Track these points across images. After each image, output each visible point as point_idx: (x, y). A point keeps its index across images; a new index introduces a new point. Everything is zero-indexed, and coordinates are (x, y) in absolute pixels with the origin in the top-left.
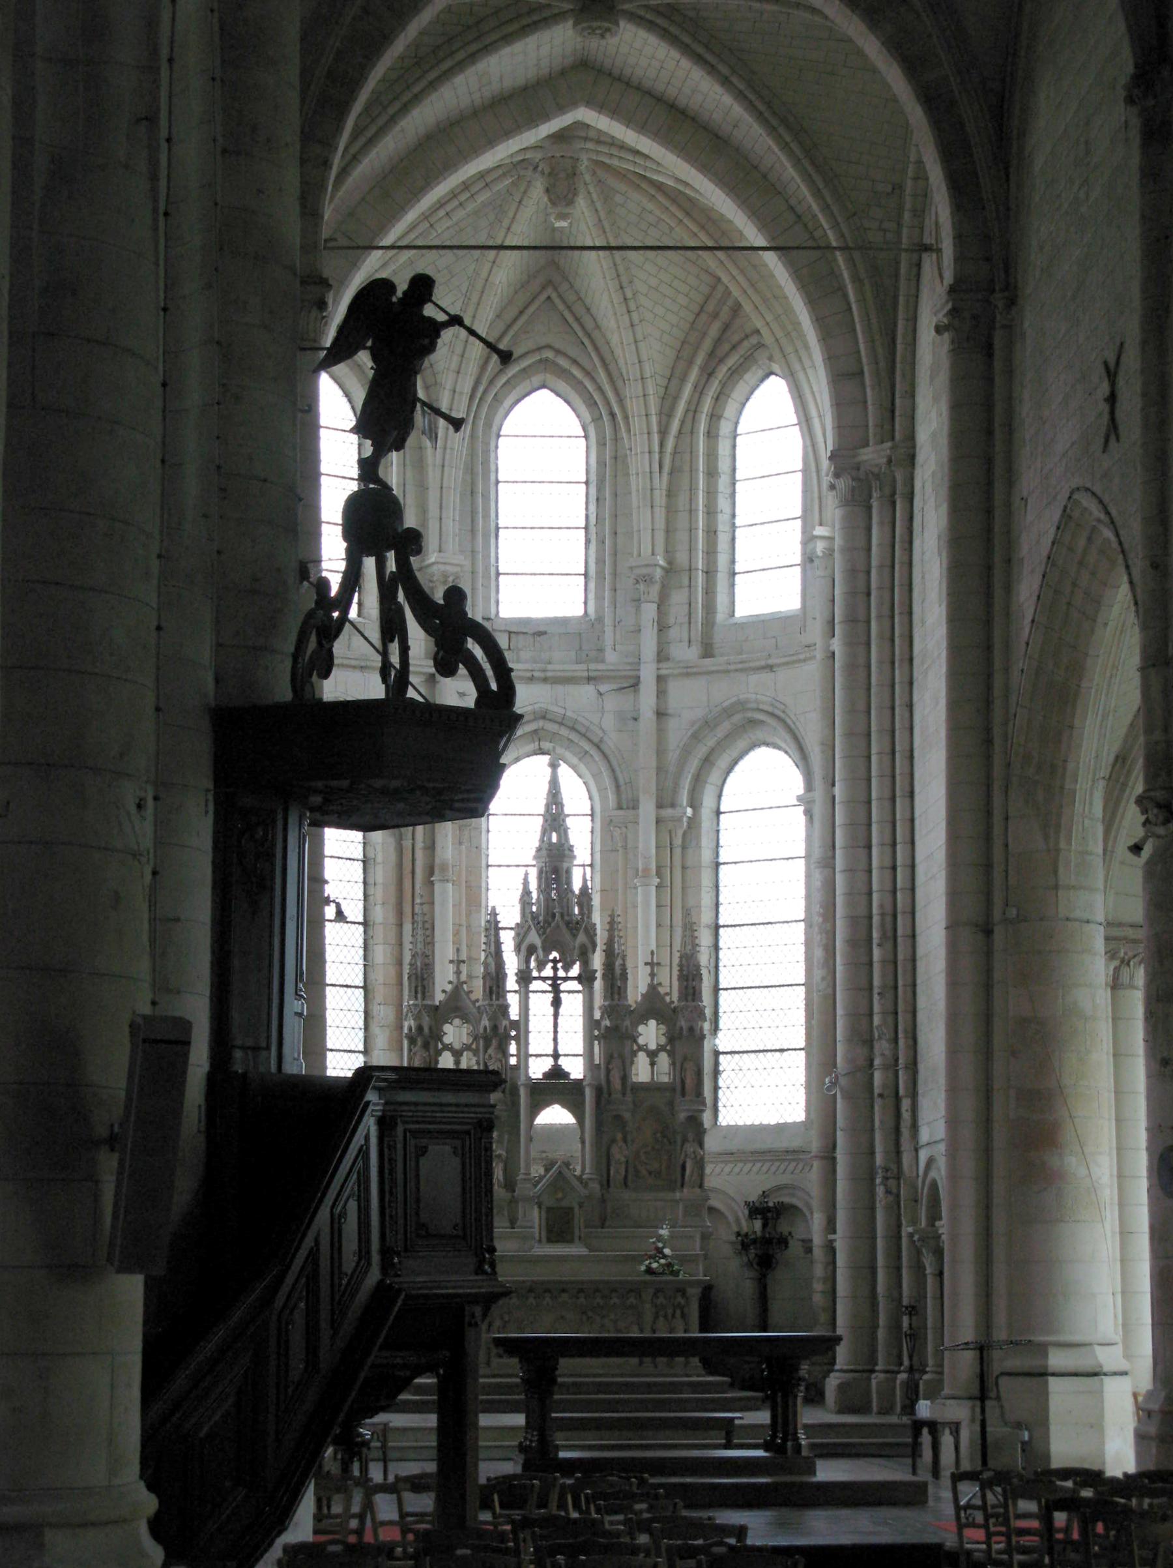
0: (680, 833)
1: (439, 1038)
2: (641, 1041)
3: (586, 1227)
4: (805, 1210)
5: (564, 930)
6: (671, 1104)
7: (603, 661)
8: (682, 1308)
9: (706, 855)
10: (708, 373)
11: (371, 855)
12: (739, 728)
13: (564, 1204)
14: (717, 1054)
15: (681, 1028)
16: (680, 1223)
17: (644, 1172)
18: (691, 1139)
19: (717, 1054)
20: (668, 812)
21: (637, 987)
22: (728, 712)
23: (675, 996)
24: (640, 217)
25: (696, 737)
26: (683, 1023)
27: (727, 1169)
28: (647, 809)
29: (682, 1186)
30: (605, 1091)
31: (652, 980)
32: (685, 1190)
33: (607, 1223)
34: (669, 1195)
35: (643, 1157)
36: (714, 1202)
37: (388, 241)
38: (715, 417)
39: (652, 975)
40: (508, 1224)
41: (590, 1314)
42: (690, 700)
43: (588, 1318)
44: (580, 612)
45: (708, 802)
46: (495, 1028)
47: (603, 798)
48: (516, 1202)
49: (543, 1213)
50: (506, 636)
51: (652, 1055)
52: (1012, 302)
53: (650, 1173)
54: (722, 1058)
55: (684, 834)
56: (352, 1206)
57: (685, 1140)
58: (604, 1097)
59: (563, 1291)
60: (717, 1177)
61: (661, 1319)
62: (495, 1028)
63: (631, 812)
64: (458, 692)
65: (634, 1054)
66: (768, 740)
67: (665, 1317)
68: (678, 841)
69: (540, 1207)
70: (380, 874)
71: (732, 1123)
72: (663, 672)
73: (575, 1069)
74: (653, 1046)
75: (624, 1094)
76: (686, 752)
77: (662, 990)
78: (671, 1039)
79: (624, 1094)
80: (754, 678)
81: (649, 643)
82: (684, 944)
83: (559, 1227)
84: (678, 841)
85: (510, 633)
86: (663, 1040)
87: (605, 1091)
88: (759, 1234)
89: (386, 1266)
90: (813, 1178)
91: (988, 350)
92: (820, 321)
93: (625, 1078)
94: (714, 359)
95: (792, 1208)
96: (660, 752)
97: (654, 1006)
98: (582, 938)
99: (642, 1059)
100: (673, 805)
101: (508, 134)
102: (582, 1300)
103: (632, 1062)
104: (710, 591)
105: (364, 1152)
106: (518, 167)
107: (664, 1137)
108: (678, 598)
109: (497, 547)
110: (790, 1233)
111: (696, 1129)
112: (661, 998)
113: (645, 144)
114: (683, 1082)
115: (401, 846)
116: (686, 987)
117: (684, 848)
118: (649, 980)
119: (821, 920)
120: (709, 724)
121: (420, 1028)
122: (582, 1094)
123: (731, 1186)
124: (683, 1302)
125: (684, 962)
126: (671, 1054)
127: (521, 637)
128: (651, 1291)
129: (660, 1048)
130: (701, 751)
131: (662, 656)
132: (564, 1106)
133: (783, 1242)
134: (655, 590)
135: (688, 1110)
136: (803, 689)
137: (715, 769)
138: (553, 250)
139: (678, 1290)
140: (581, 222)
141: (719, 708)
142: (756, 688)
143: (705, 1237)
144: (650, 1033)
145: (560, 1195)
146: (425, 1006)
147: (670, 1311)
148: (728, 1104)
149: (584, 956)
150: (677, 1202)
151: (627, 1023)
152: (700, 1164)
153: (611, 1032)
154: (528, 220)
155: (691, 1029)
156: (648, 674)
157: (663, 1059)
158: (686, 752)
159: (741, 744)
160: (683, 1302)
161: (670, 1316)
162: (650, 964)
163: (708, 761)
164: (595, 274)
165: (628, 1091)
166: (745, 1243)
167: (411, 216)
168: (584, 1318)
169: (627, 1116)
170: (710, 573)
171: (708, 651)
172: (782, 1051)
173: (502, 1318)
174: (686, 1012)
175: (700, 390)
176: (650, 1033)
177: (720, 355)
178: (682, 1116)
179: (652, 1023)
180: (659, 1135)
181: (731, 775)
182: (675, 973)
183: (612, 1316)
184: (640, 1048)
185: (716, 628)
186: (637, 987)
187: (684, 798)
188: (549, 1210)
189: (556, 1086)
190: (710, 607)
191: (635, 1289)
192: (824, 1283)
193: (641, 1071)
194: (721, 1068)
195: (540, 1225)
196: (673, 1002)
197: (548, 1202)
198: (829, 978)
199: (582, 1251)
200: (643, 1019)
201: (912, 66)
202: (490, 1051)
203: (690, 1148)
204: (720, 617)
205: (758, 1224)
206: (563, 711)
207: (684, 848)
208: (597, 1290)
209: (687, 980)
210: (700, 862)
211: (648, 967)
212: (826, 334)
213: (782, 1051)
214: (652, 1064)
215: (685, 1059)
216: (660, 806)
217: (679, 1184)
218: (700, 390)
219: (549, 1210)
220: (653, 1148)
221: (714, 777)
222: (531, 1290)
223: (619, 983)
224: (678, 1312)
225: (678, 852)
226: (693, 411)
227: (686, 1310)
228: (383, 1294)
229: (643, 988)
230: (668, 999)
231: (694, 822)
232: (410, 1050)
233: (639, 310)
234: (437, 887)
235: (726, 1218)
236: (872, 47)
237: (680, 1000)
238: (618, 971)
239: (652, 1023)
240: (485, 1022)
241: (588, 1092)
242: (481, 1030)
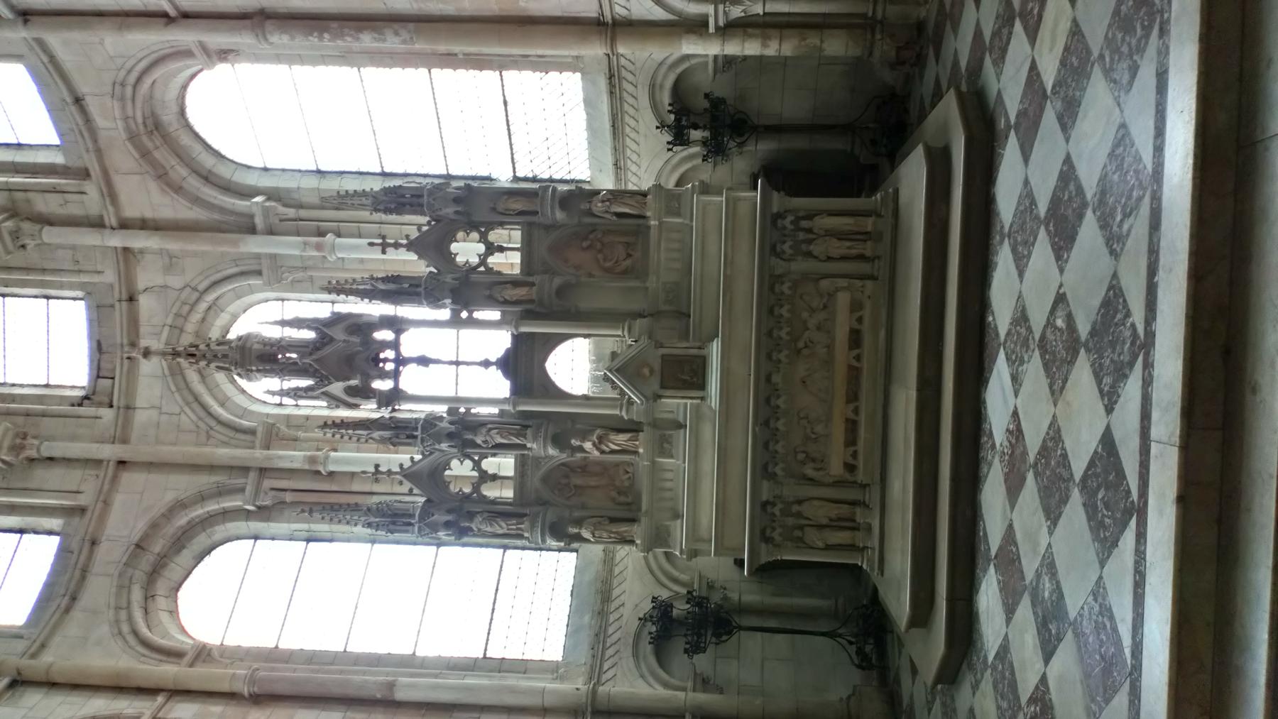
0: (281, 209)
1: (467, 497)
2: (475, 260)
3: (687, 339)
4: (679, 70)
5: (328, 350)
6: (549, 228)
7: (112, 286)
8: (799, 219)
9: (312, 182)
11: (305, 534)
12: (164, 140)
13: (657, 366)
14: (516, 179)
15: (456, 212)
16: (687, 222)
17: (628, 262)
18: (588, 206)
19: (516, 179)
20: (259, 221)
21: (411, 264)
22: (145, 154)
23: (423, 220)
26: (449, 211)
27: (634, 168)
28: (255, 245)
29: (644, 217)
30: (529, 307)
31: (401, 245)
32: (649, 214)
33: (685, 310)
34: (653, 234)
35: (608, 264)
36: (671, 185)
39: (397, 246)
40: (682, 431)
41: (801, 344)
43: (806, 347)
44: (81, 305)
45: (251, 180)
46: (450, 436)
47: (252, 291)
48: (655, 420)
49: (668, 393)
50: (101, 381)
51: (491, 249)
53: (629, 256)
54: (520, 174)
55: (285, 205)
57: (590, 213)
59: (768, 379)
60: (642, 178)
61: (812, 247)
62: (450, 436)
63: (263, 261)
65: (489, 271)
66: (175, 109)
67: (810, 242)
68: (291, 212)
69: (660, 397)
70: (322, 528)
71: (587, 164)
72: (114, 222)
73: (499, 342)
74: (481, 248)
75: (533, 284)
76: (197, 201)
77: (414, 233)
78: (471, 226)
79: (533, 284)
80: (100, 122)
81: (90, 238)
82: (362, 207)
83: (686, 374)
84: (291, 212)
85: (98, 377)
86: (475, 235)
87: (529, 307)
88: (707, 134)
90: (643, 55)
93: (515, 283)
95: (677, 89)
97: (434, 245)
98: (338, 334)
99: (495, 260)
100: (252, 216)
102: (782, 356)
103: (499, 273)
107: (586, 238)
109: (22, 386)
110: (707, 96)
112: (423, 235)
114: (521, 213)
115: (292, 503)
116: (412, 205)
117: (301, 206)
118: (403, 250)
119: (326, 35)
121: (447, 525)
122: (532, 335)
123: (651, 163)
124: (790, 218)
125: (381, 207)
126: (491, 226)
127: (103, 365)
128: (774, 261)
129: (483, 239)
130: (193, 183)
131: (97, 224)
132: (545, 360)
133: (716, 103)
134: (26, 226)
135: (552, 208)
137: (215, 170)
139: (774, 223)
141: (141, 161)
143: (705, 189)
144: (467, 250)
145: (646, 371)
146: (422, 518)
147: (801, 236)
148: (567, 169)
150: (661, 223)
151: (448, 279)
153: (463, 291)
155: (457, 200)
156: (116, 240)
157: (496, 236)
158: (197, 201)
159: (186, 140)
160: (790, 218)
161: (811, 236)
162: (384, 247)
163: (208, 178)
165: (531, 279)
166: (715, 150)
168: (805, 352)
169: (557, 281)
172: (505, 103)
173: (803, 463)
174: (458, 205)
176: (467, 250)
178: (560, 215)
179: (454, 247)
180: (585, 244)
181: (223, 153)
182: (393, 217)
183: (805, 315)
184: (483, 262)
185: (70, 165)
186: (411, 264)
187: (241, 204)
188: (663, 387)
189: (523, 365)
192: (769, 38)
193: (509, 262)
194: (530, 175)
195: (683, 398)
196: (429, 223)
197: (654, 385)
198: (396, 26)
199: (715, 349)
200: (450, 258)
202: (479, 441)
203: (598, 207)
204: (58, 159)
205: (696, 134)
206: (167, 329)
207: (301, 206)
208: (770, 334)
209: (404, 205)
210: (313, 189)
211: (388, 250)
213: (505, 103)
214: (501, 249)
215: (494, 209)
216: (252, 230)
217: (641, 221)
219: (663, 387)
220: (600, 251)
221: (224, 171)
222: (766, 423)
223: (406, 286)
224: (804, 224)
225: (303, 213)
227: (801, 214)
229: (413, 257)
230: (425, 228)
232: (475, 536)
234: (332, 468)
235: (687, 171)
237: (423, 214)
238: (391, 286)
239: (454, 247)
240: (444, 446)
241: (524, 329)
242: (455, 450)
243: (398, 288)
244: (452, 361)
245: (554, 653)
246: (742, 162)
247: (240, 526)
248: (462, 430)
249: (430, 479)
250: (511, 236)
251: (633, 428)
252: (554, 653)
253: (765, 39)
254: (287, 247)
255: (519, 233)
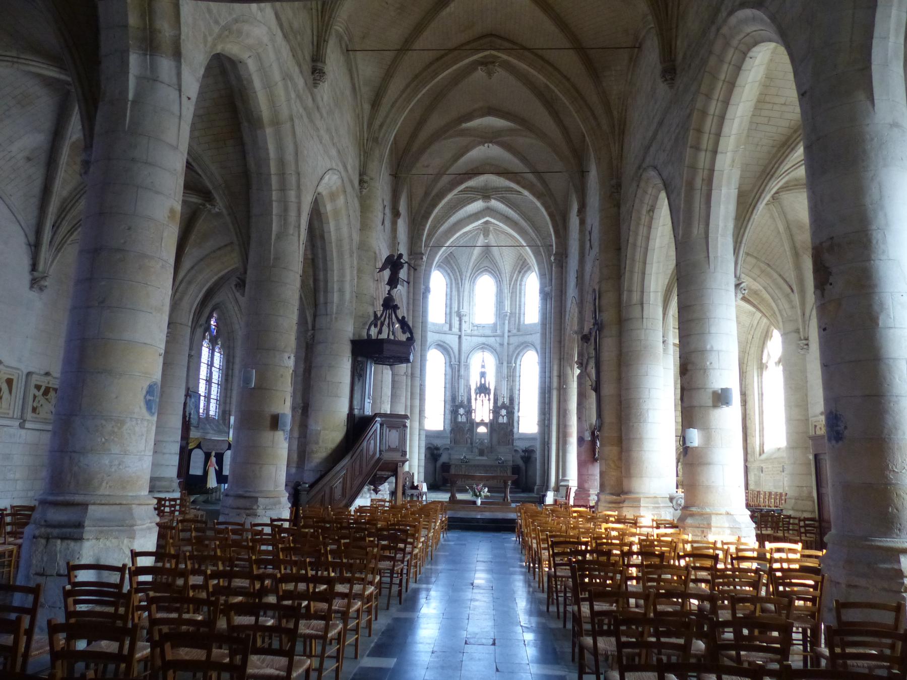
9: (518, 374)
10: (520, 272)
21: (499, 404)
22: (522, 344)
24: (503, 240)
25: (516, 349)
28: (505, 364)
37: (447, 244)
38: (521, 280)
42: (515, 341)
45: (518, 363)
52: (566, 257)
56: (372, 442)
58: (493, 426)
60: (516, 443)
64: (403, 337)
76: (514, 352)
83: (481, 453)
89: (380, 454)
91: (562, 267)
92: (537, 261)
94: (521, 269)
96: (508, 351)
97: (504, 406)
101: (472, 223)
104: (519, 318)
105: (376, 430)
106: (477, 229)
108: (513, 319)
111: (512, 432)
113: (501, 224)
120: (518, 346)
136: (537, 339)
138: (487, 246)
140: (492, 239)
142: (529, 338)
144: (461, 411)
149: (489, 394)
152: (513, 440)
153: (496, 411)
154: (481, 241)
158: (514, 352)
163: (518, 354)
164: (495, 251)
166: (522, 458)
167: (451, 240)
170: (520, 314)
171: (519, 330)
175: (518, 276)
176: (504, 412)
177: (522, 267)
186: (499, 404)
189: (482, 423)
190: (519, 321)
191: (497, 467)
193: (501, 420)
201: (547, 208)
212: (538, 264)
218: (518, 276)
226: (516, 280)
228: (379, 459)
231: (515, 367)
233: (506, 259)
236: (539, 204)
243: (496, 401)
244: (482, 411)
245: (520, 431)
246: (520, 463)
247: (448, 361)
248: (469, 412)
249: (461, 405)
250: (505, 420)
251: (471, 444)
252: (520, 431)
253: (229, 214)
254: (505, 371)
255: (805, 195)
